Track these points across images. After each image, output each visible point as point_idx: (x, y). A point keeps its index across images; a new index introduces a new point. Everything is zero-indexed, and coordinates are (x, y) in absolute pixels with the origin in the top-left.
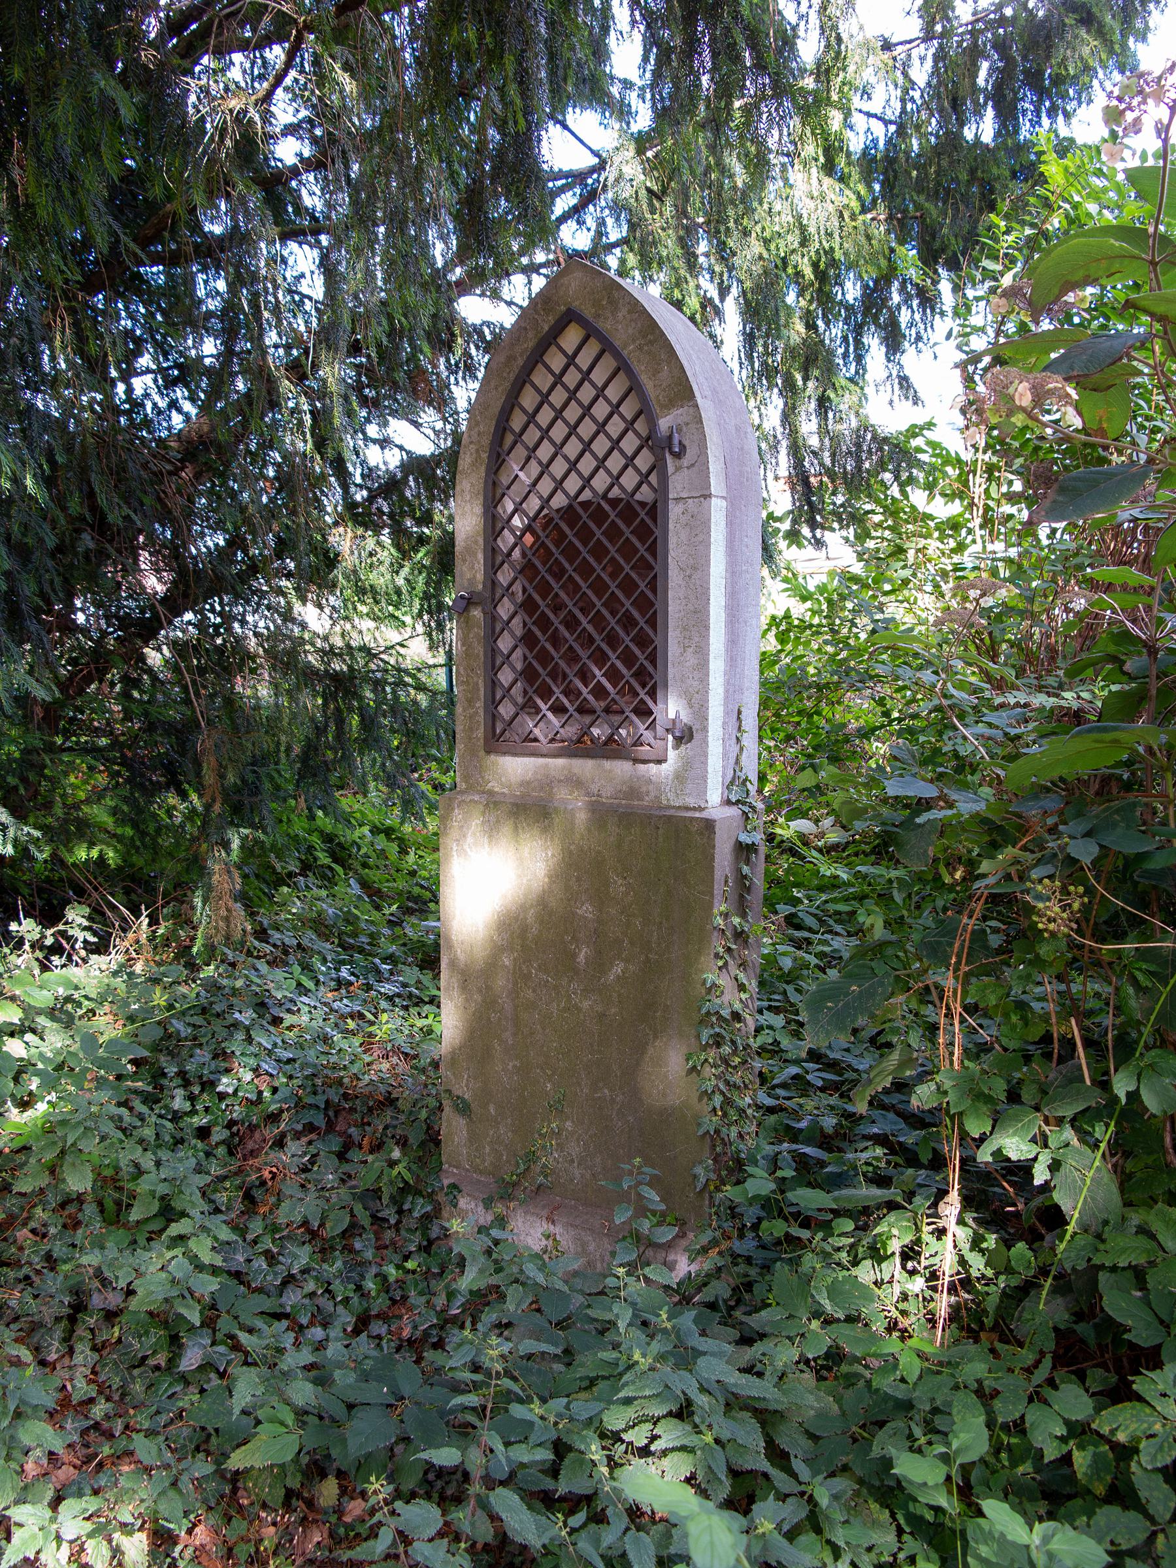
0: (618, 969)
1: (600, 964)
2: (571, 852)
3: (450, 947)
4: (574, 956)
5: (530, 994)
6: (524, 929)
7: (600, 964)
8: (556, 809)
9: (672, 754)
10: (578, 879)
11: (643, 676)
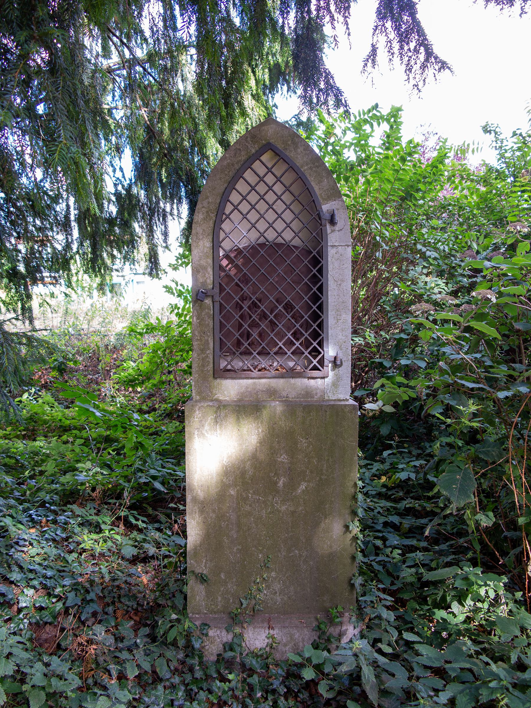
0: (303, 486)
1: (292, 485)
2: (274, 429)
3: (192, 490)
4: (276, 483)
6: (243, 473)
7: (292, 485)
9: (331, 374)
10: (279, 442)
11: (316, 335)
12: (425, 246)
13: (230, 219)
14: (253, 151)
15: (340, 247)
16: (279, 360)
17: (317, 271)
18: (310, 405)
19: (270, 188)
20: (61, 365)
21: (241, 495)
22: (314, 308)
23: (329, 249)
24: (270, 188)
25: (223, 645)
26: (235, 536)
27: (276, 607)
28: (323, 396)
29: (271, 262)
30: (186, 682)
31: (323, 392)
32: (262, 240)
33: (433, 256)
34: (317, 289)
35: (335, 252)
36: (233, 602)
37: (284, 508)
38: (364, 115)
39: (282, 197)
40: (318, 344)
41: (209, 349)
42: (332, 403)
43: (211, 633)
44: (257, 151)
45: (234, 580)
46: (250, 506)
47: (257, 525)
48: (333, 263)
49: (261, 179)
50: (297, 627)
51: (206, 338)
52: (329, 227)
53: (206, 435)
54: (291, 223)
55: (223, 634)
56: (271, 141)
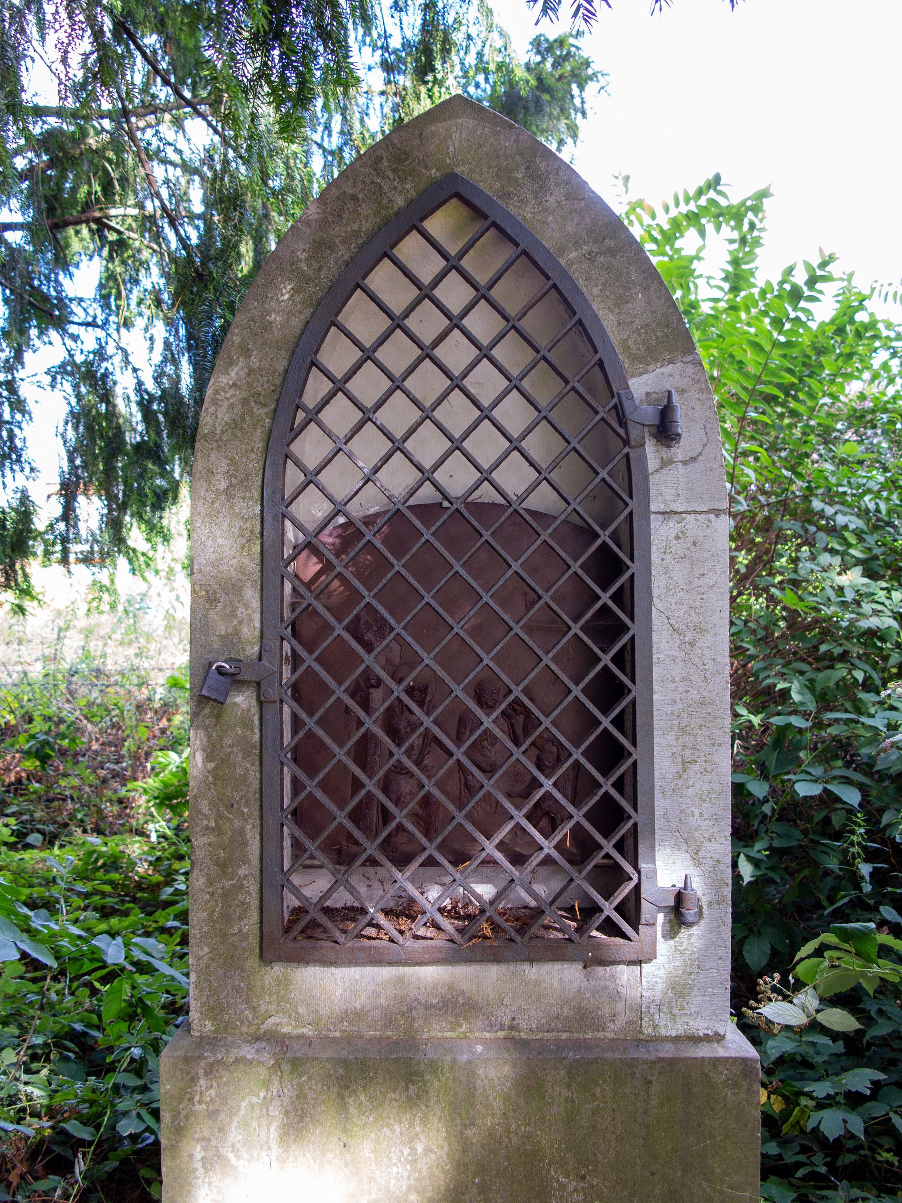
8: (434, 1067)
9: (663, 947)
12: (831, 503)
13: (320, 425)
14: (400, 202)
15: (690, 518)
17: (612, 598)
19: (455, 323)
20: (43, 747)
22: (606, 722)
23: (655, 522)
24: (455, 323)
28: (635, 1024)
29: (457, 567)
31: (639, 1011)
32: (426, 494)
33: (852, 527)
34: (613, 660)
35: (673, 533)
38: (687, 202)
39: (495, 352)
40: (619, 847)
41: (246, 861)
42: (668, 1051)
44: (410, 203)
48: (667, 571)
49: (426, 293)
51: (237, 823)
52: (652, 452)
53: (234, 1161)
54: (523, 437)
56: (457, 170)
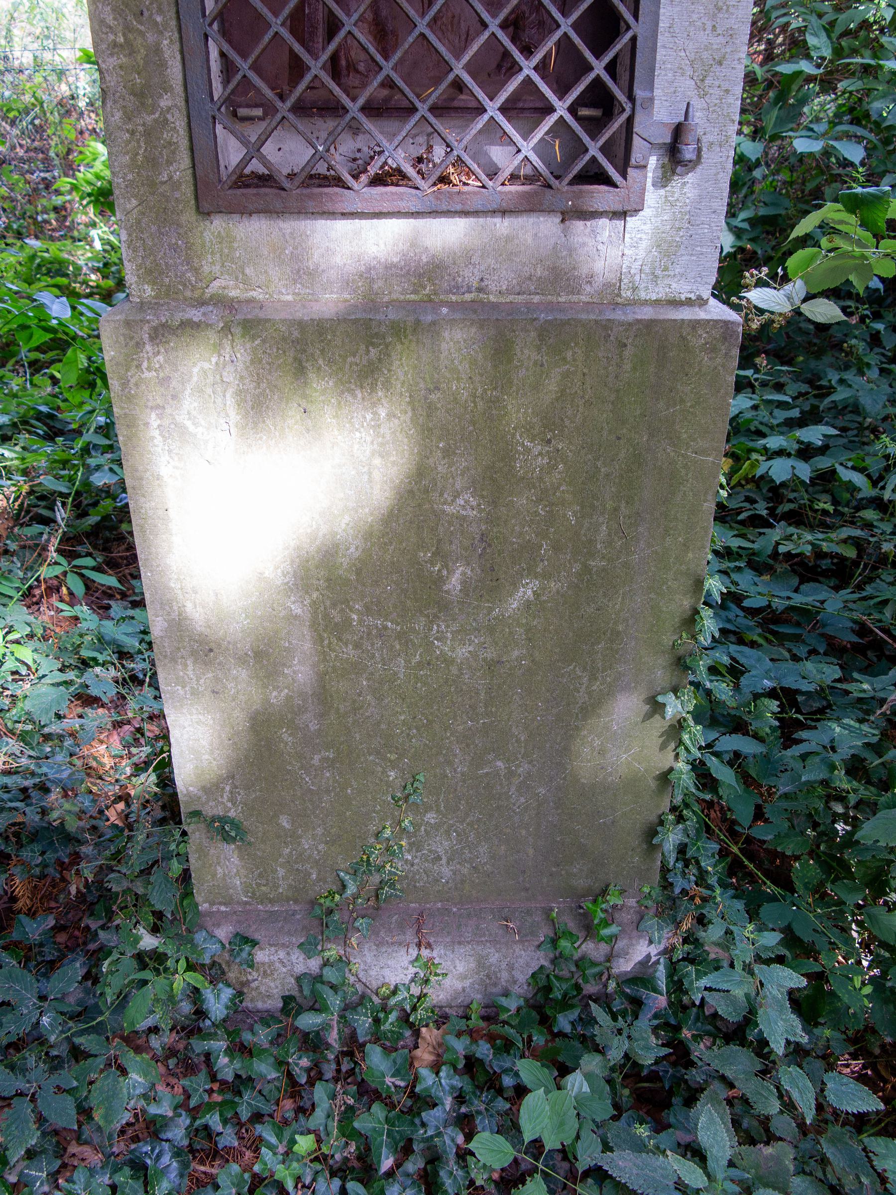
0: (527, 591)
4: (440, 581)
5: (350, 652)
10: (448, 453)
16: (451, 138)
18: (567, 322)
21: (326, 616)
25: (298, 979)
26: (313, 726)
27: (437, 888)
30: (193, 1103)
36: (319, 880)
37: (462, 652)
41: (167, 88)
42: (647, 313)
43: (261, 956)
45: (319, 831)
46: (357, 646)
47: (380, 699)
50: (494, 942)
55: (293, 958)
